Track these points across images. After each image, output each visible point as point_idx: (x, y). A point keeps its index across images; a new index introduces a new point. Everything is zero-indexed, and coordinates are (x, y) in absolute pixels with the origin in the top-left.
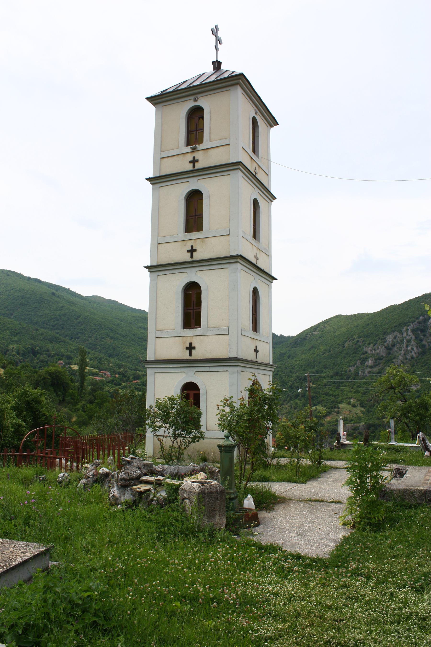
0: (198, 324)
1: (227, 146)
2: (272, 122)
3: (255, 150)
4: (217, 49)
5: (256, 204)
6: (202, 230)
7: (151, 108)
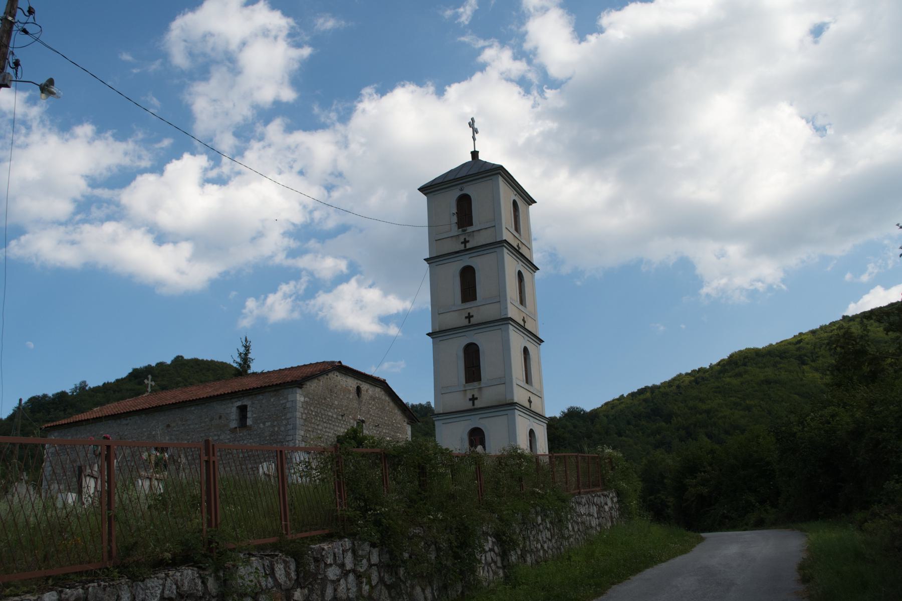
0: (479, 379)
1: (493, 229)
2: (530, 201)
3: (517, 229)
4: (474, 139)
5: (520, 275)
6: (480, 380)
7: (423, 198)
